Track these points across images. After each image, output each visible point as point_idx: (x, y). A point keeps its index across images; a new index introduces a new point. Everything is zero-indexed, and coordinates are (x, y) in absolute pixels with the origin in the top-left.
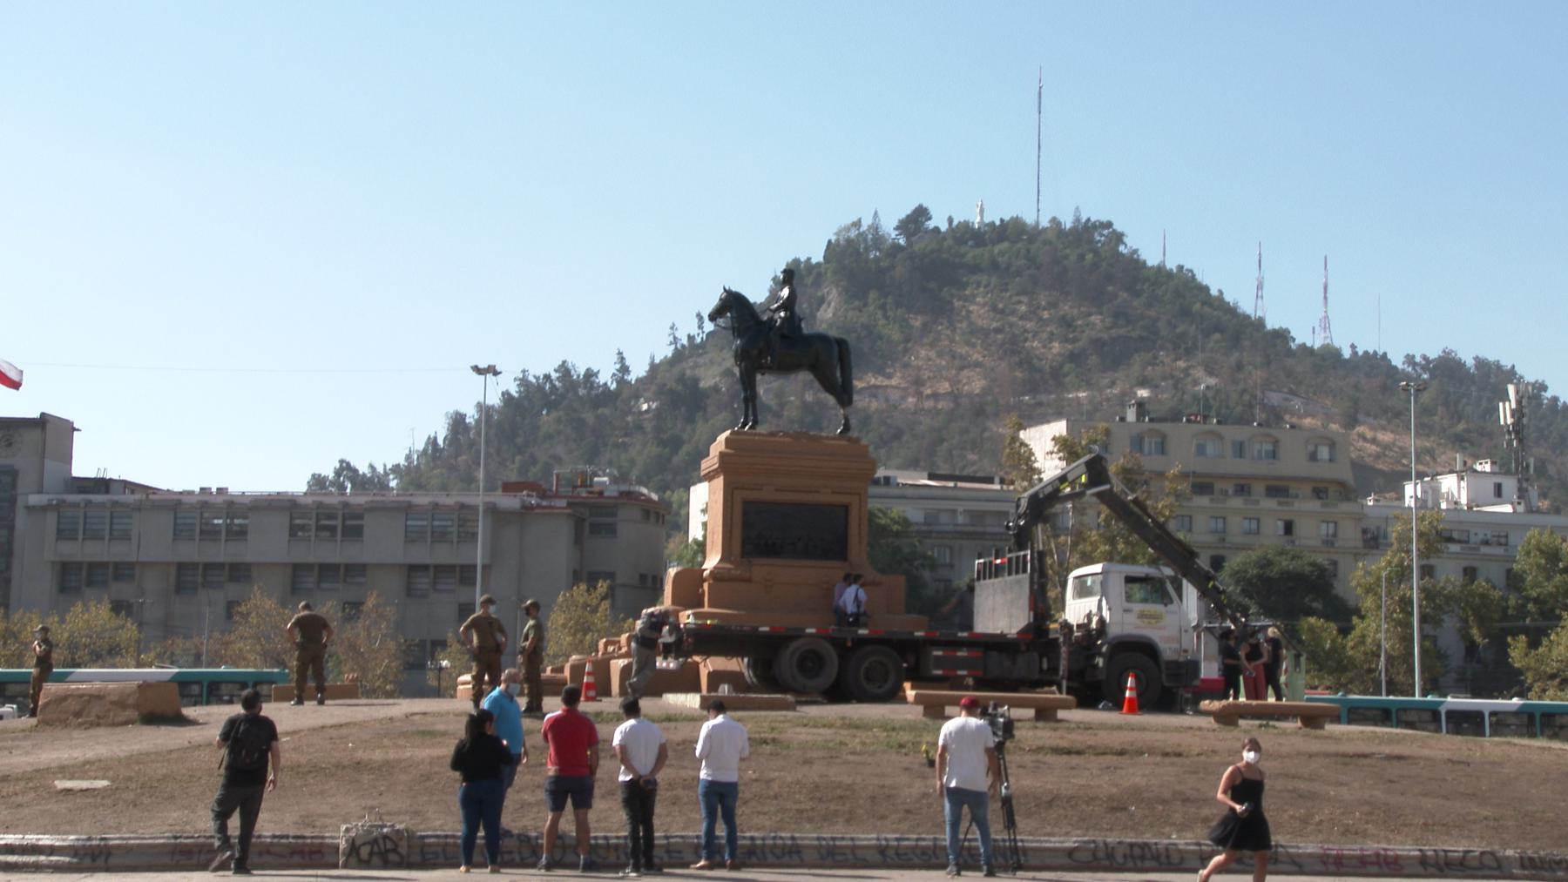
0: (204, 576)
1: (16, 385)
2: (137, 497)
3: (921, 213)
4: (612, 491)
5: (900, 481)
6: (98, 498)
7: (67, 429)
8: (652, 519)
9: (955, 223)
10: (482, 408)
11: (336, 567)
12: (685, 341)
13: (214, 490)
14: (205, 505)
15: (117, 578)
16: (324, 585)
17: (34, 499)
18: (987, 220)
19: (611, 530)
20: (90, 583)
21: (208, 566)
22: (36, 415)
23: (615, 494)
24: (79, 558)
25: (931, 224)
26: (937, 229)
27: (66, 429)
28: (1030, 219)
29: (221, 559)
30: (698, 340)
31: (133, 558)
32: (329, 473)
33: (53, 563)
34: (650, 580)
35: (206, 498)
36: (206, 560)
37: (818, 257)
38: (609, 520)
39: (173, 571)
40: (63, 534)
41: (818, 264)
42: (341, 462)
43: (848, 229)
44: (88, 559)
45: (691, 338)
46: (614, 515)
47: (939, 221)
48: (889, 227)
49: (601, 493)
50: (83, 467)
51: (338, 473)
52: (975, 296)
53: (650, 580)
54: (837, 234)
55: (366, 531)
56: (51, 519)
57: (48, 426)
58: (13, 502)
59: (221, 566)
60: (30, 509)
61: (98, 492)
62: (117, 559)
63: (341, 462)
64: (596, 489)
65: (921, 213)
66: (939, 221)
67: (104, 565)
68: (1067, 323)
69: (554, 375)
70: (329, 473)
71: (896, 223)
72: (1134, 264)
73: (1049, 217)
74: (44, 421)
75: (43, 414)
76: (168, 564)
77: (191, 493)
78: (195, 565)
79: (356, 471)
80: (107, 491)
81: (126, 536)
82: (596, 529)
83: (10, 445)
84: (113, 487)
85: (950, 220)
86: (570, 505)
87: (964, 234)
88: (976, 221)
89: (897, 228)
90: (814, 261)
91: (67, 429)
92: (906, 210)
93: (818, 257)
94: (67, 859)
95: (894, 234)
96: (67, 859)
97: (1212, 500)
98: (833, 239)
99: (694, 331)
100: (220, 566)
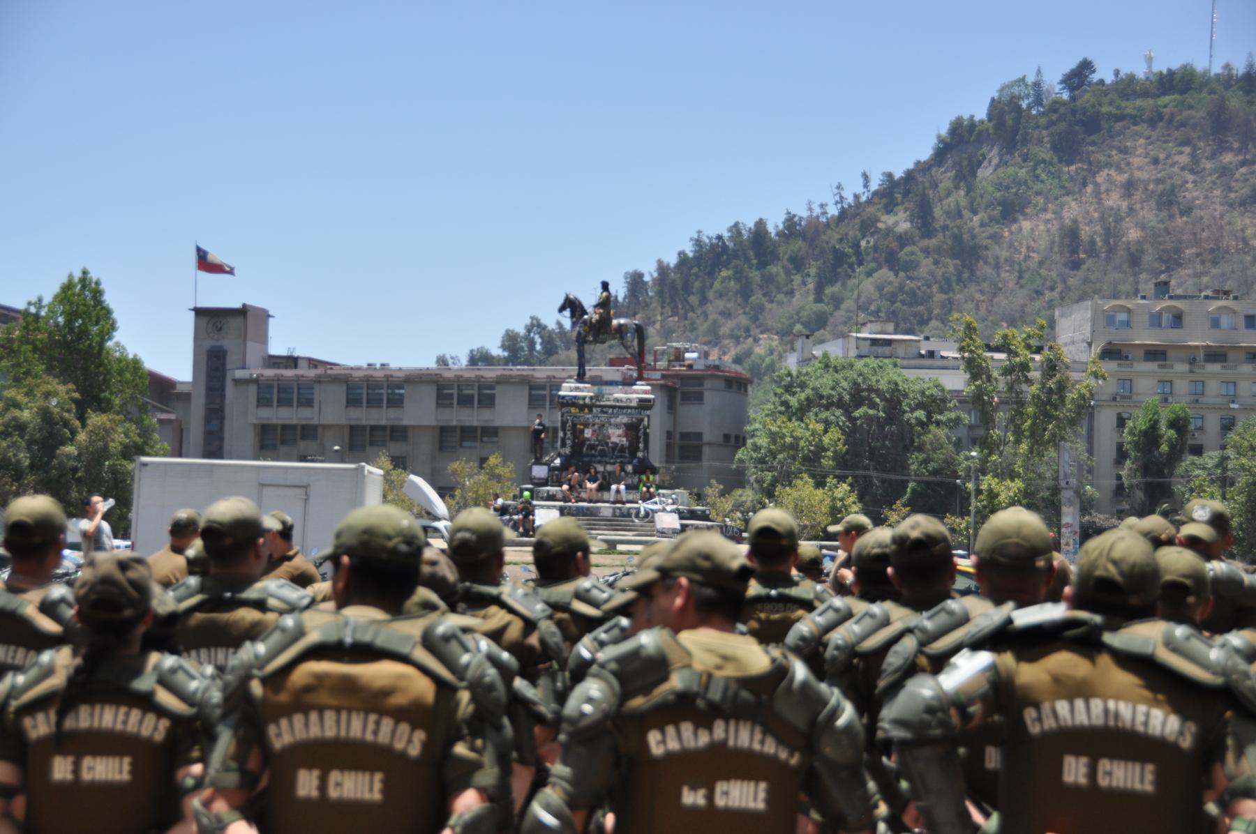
0: (371, 435)
1: (231, 272)
2: (319, 371)
3: (1085, 67)
4: (699, 366)
5: (944, 354)
6: (288, 373)
7: (264, 316)
8: (735, 387)
9: (1122, 74)
10: (663, 269)
11: (474, 429)
12: (851, 200)
13: (378, 366)
14: (368, 379)
15: (303, 437)
16: (465, 444)
17: (240, 374)
18: (1156, 69)
19: (699, 398)
20: (283, 442)
21: (374, 428)
22: (237, 305)
23: (702, 367)
24: (274, 421)
25: (1095, 77)
26: (1102, 82)
27: (263, 316)
28: (1200, 65)
29: (383, 422)
30: (864, 199)
31: (315, 422)
32: (521, 331)
33: (255, 425)
34: (733, 440)
35: (370, 373)
36: (372, 423)
37: (981, 114)
38: (697, 389)
39: (347, 431)
40: (263, 402)
41: (982, 122)
42: (532, 318)
43: (1010, 86)
44: (280, 422)
45: (856, 197)
46: (701, 385)
47: (1104, 73)
48: (1053, 81)
49: (690, 367)
50: (277, 348)
51: (529, 330)
52: (1135, 148)
53: (733, 440)
54: (1002, 90)
55: (497, 401)
56: (253, 389)
57: (249, 314)
58: (224, 376)
59: (383, 428)
60: (237, 382)
61: (286, 367)
62: (304, 422)
63: (532, 318)
64: (687, 363)
65: (1085, 67)
66: (1104, 73)
67: (294, 427)
68: (1225, 172)
69: (726, 235)
70: (521, 331)
71: (1060, 77)
72: (53, 496)
73: (1223, 63)
74: (243, 312)
75: (244, 305)
76: (343, 426)
77: (359, 369)
78: (363, 428)
79: (545, 328)
80: (296, 367)
81: (307, 402)
82: (687, 397)
83: (220, 329)
84: (300, 363)
85: (1117, 73)
86: (664, 377)
87: (1127, 87)
88: (1140, 72)
89: (1062, 82)
90: (977, 119)
91: (264, 316)
92: (1071, 64)
93: (981, 114)
94: (770, 747)
95: (1058, 88)
96: (770, 747)
97: (1223, 367)
98: (996, 95)
99: (860, 189)
100: (383, 428)
